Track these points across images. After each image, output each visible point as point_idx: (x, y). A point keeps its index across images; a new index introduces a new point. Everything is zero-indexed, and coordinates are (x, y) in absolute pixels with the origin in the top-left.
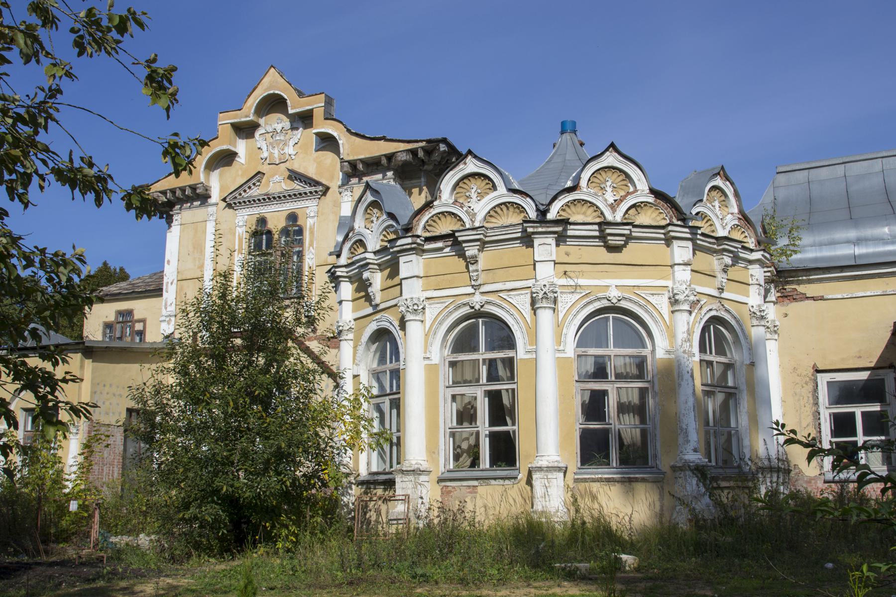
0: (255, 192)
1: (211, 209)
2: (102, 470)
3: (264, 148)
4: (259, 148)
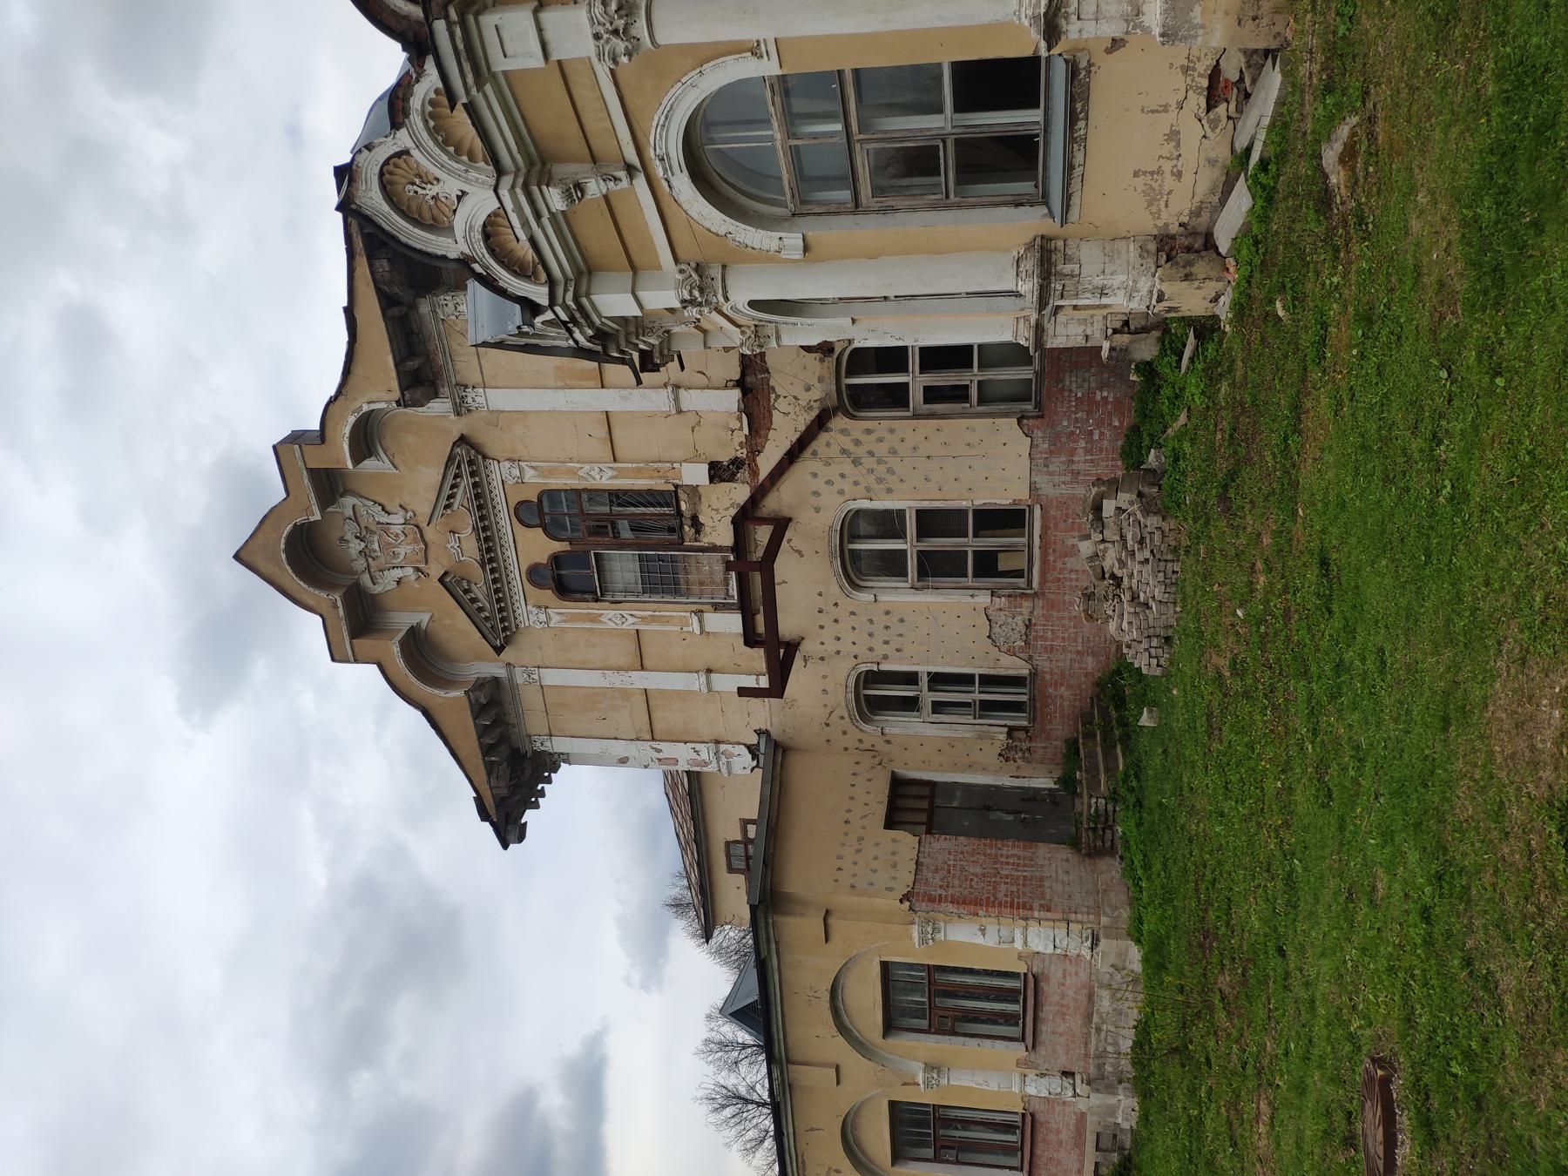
2: (1007, 877)
3: (398, 573)
4: (398, 583)
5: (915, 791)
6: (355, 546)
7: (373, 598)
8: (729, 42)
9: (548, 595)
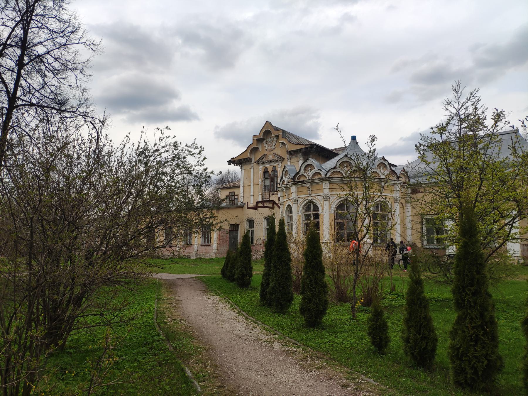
5: (237, 228)
6: (270, 140)
7: (263, 142)
9: (264, 170)
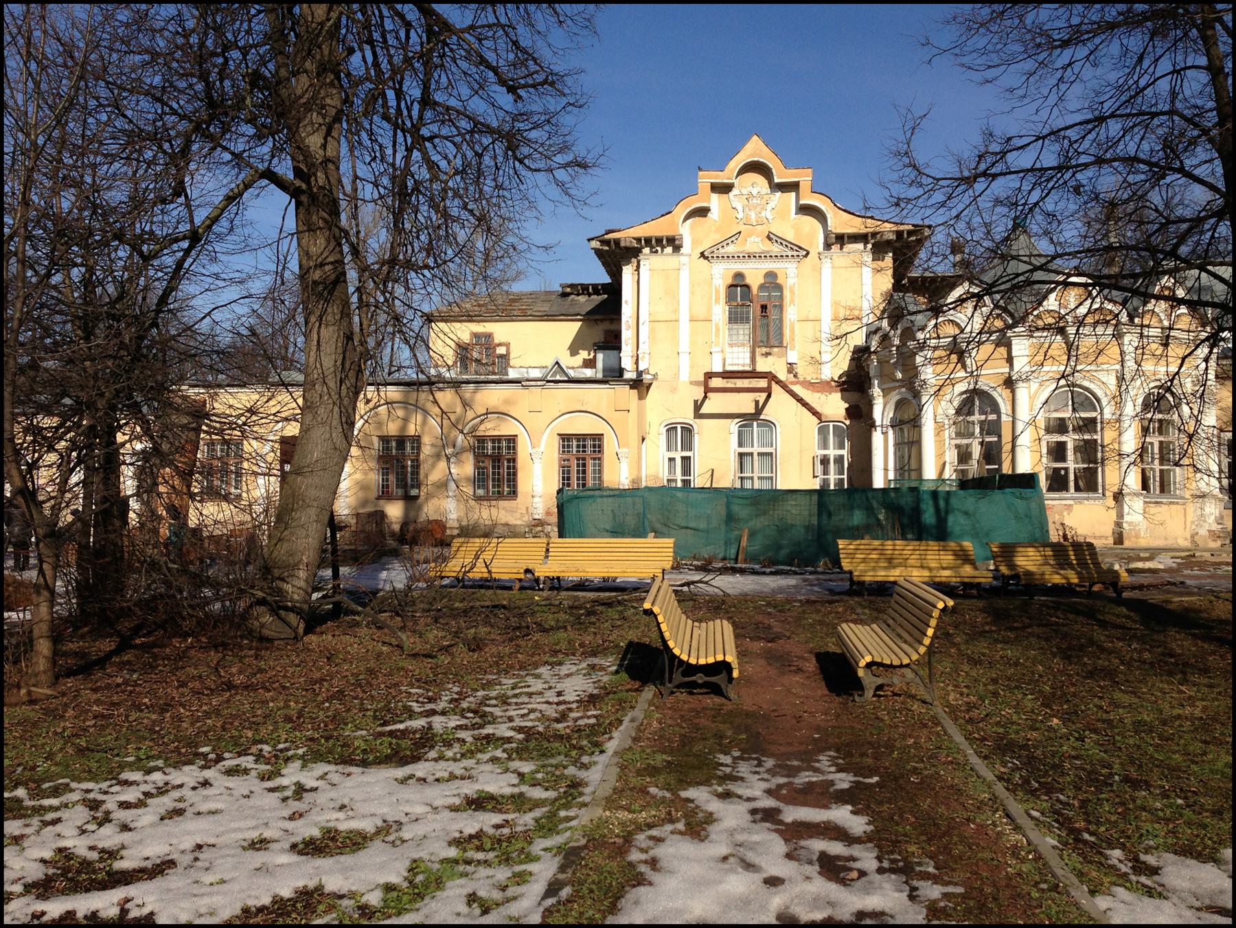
0: (731, 249)
1: (683, 259)
3: (740, 209)
8: (830, 879)
